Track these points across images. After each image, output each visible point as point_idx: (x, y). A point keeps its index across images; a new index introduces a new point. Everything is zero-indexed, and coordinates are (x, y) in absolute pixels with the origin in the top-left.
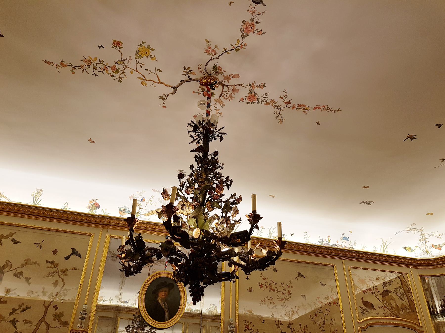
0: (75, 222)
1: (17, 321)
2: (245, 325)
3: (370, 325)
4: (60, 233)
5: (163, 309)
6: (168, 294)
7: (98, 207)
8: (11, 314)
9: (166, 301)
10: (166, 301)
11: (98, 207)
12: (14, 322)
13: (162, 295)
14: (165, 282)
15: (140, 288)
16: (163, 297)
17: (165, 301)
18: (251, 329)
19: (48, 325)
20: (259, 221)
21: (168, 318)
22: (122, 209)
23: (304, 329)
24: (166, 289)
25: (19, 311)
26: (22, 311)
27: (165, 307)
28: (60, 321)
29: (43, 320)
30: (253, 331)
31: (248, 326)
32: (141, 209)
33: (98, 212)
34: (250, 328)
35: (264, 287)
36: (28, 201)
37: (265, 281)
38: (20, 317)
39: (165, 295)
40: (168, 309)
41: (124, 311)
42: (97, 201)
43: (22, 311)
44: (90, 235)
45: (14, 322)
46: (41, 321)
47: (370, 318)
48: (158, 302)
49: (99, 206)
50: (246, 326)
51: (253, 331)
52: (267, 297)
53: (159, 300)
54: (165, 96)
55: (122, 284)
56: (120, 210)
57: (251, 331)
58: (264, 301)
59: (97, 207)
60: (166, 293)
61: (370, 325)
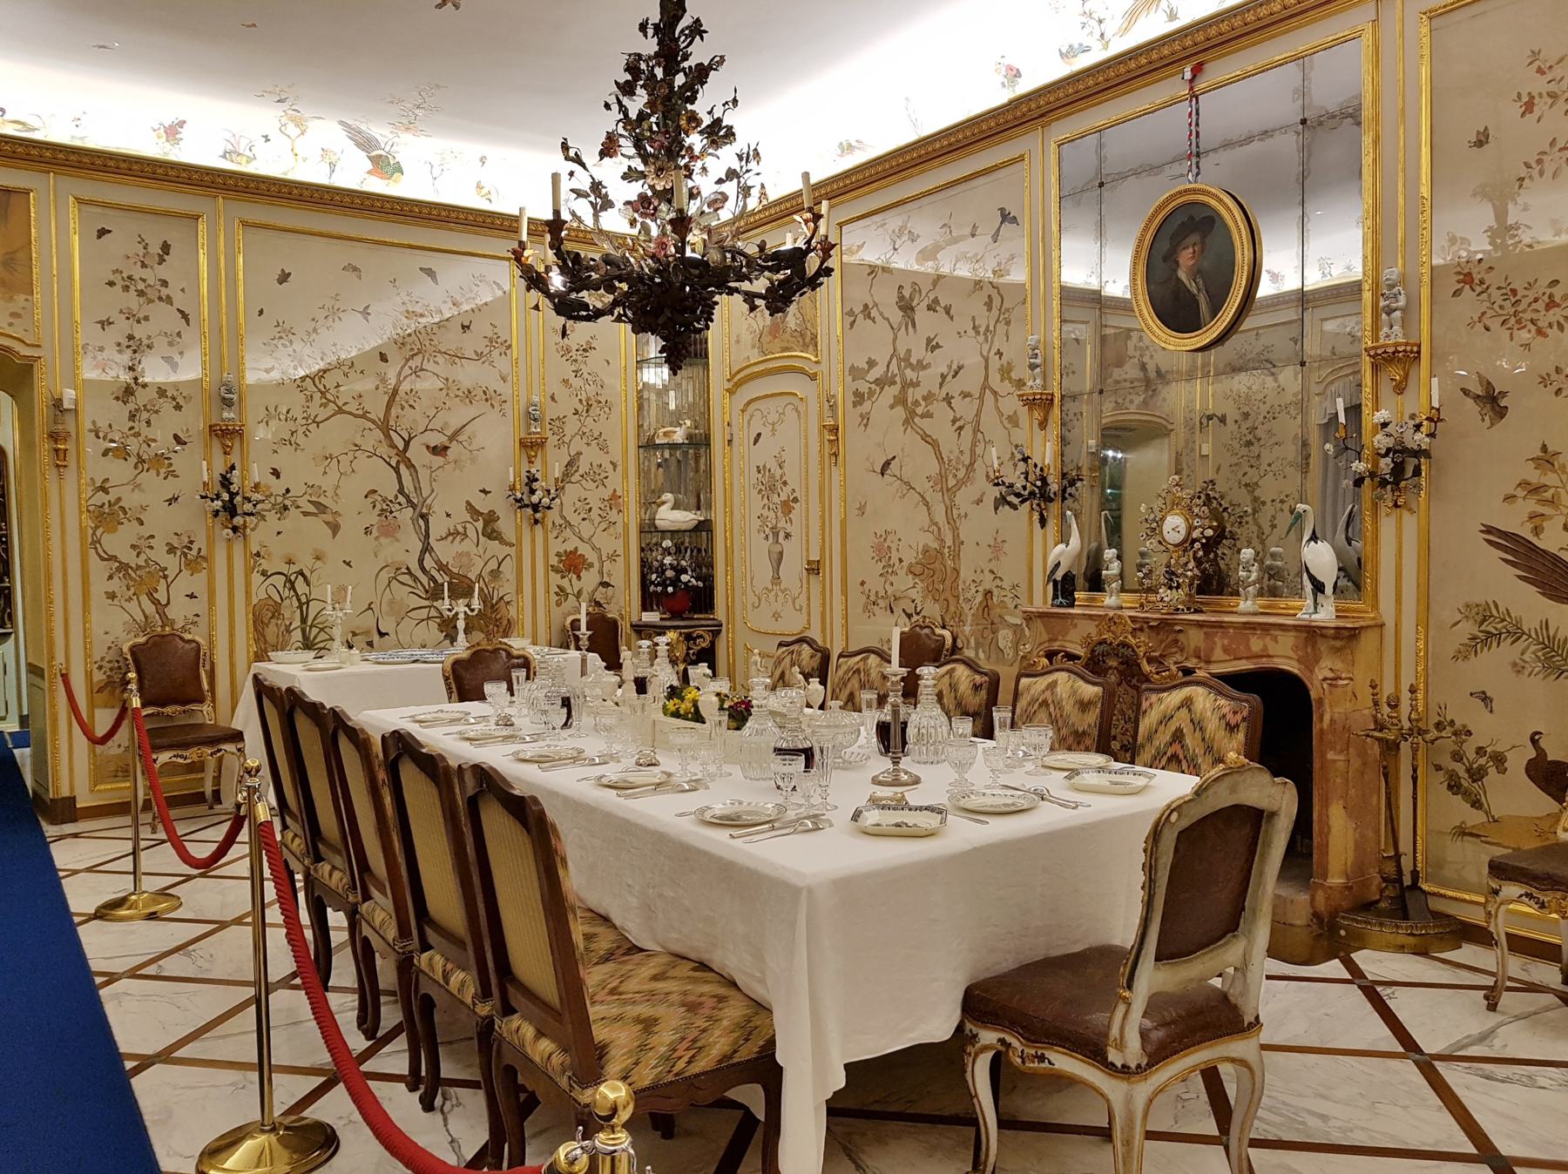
0: (989, 140)
1: (952, 397)
4: (973, 181)
5: (1194, 296)
6: (1202, 251)
7: (1018, 74)
8: (941, 385)
9: (1199, 271)
11: (1018, 74)
12: (948, 399)
13: (1186, 258)
14: (1191, 218)
15: (1137, 231)
17: (1196, 273)
18: (1482, 282)
19: (995, 393)
20: (1461, 947)
21: (1208, 319)
22: (1064, 51)
25: (950, 377)
26: (954, 377)
27: (1199, 290)
28: (1010, 379)
29: (985, 386)
30: (1488, 288)
31: (1470, 274)
32: (1100, 22)
33: (1025, 86)
34: (1477, 277)
35: (1541, 106)
36: (992, 96)
37: (1549, 76)
38: (953, 387)
39: (1193, 258)
40: (1207, 292)
41: (1116, 308)
42: (1006, 61)
43: (954, 377)
44: (1021, 158)
45: (948, 399)
46: (984, 388)
48: (1179, 280)
49: (1018, 70)
50: (1462, 277)
51: (1488, 288)
52: (1551, 144)
53: (1182, 275)
54: (543, 708)
55: (1101, 235)
56: (1061, 54)
57: (1479, 289)
58: (1539, 162)
59: (1015, 76)
60: (1196, 249)
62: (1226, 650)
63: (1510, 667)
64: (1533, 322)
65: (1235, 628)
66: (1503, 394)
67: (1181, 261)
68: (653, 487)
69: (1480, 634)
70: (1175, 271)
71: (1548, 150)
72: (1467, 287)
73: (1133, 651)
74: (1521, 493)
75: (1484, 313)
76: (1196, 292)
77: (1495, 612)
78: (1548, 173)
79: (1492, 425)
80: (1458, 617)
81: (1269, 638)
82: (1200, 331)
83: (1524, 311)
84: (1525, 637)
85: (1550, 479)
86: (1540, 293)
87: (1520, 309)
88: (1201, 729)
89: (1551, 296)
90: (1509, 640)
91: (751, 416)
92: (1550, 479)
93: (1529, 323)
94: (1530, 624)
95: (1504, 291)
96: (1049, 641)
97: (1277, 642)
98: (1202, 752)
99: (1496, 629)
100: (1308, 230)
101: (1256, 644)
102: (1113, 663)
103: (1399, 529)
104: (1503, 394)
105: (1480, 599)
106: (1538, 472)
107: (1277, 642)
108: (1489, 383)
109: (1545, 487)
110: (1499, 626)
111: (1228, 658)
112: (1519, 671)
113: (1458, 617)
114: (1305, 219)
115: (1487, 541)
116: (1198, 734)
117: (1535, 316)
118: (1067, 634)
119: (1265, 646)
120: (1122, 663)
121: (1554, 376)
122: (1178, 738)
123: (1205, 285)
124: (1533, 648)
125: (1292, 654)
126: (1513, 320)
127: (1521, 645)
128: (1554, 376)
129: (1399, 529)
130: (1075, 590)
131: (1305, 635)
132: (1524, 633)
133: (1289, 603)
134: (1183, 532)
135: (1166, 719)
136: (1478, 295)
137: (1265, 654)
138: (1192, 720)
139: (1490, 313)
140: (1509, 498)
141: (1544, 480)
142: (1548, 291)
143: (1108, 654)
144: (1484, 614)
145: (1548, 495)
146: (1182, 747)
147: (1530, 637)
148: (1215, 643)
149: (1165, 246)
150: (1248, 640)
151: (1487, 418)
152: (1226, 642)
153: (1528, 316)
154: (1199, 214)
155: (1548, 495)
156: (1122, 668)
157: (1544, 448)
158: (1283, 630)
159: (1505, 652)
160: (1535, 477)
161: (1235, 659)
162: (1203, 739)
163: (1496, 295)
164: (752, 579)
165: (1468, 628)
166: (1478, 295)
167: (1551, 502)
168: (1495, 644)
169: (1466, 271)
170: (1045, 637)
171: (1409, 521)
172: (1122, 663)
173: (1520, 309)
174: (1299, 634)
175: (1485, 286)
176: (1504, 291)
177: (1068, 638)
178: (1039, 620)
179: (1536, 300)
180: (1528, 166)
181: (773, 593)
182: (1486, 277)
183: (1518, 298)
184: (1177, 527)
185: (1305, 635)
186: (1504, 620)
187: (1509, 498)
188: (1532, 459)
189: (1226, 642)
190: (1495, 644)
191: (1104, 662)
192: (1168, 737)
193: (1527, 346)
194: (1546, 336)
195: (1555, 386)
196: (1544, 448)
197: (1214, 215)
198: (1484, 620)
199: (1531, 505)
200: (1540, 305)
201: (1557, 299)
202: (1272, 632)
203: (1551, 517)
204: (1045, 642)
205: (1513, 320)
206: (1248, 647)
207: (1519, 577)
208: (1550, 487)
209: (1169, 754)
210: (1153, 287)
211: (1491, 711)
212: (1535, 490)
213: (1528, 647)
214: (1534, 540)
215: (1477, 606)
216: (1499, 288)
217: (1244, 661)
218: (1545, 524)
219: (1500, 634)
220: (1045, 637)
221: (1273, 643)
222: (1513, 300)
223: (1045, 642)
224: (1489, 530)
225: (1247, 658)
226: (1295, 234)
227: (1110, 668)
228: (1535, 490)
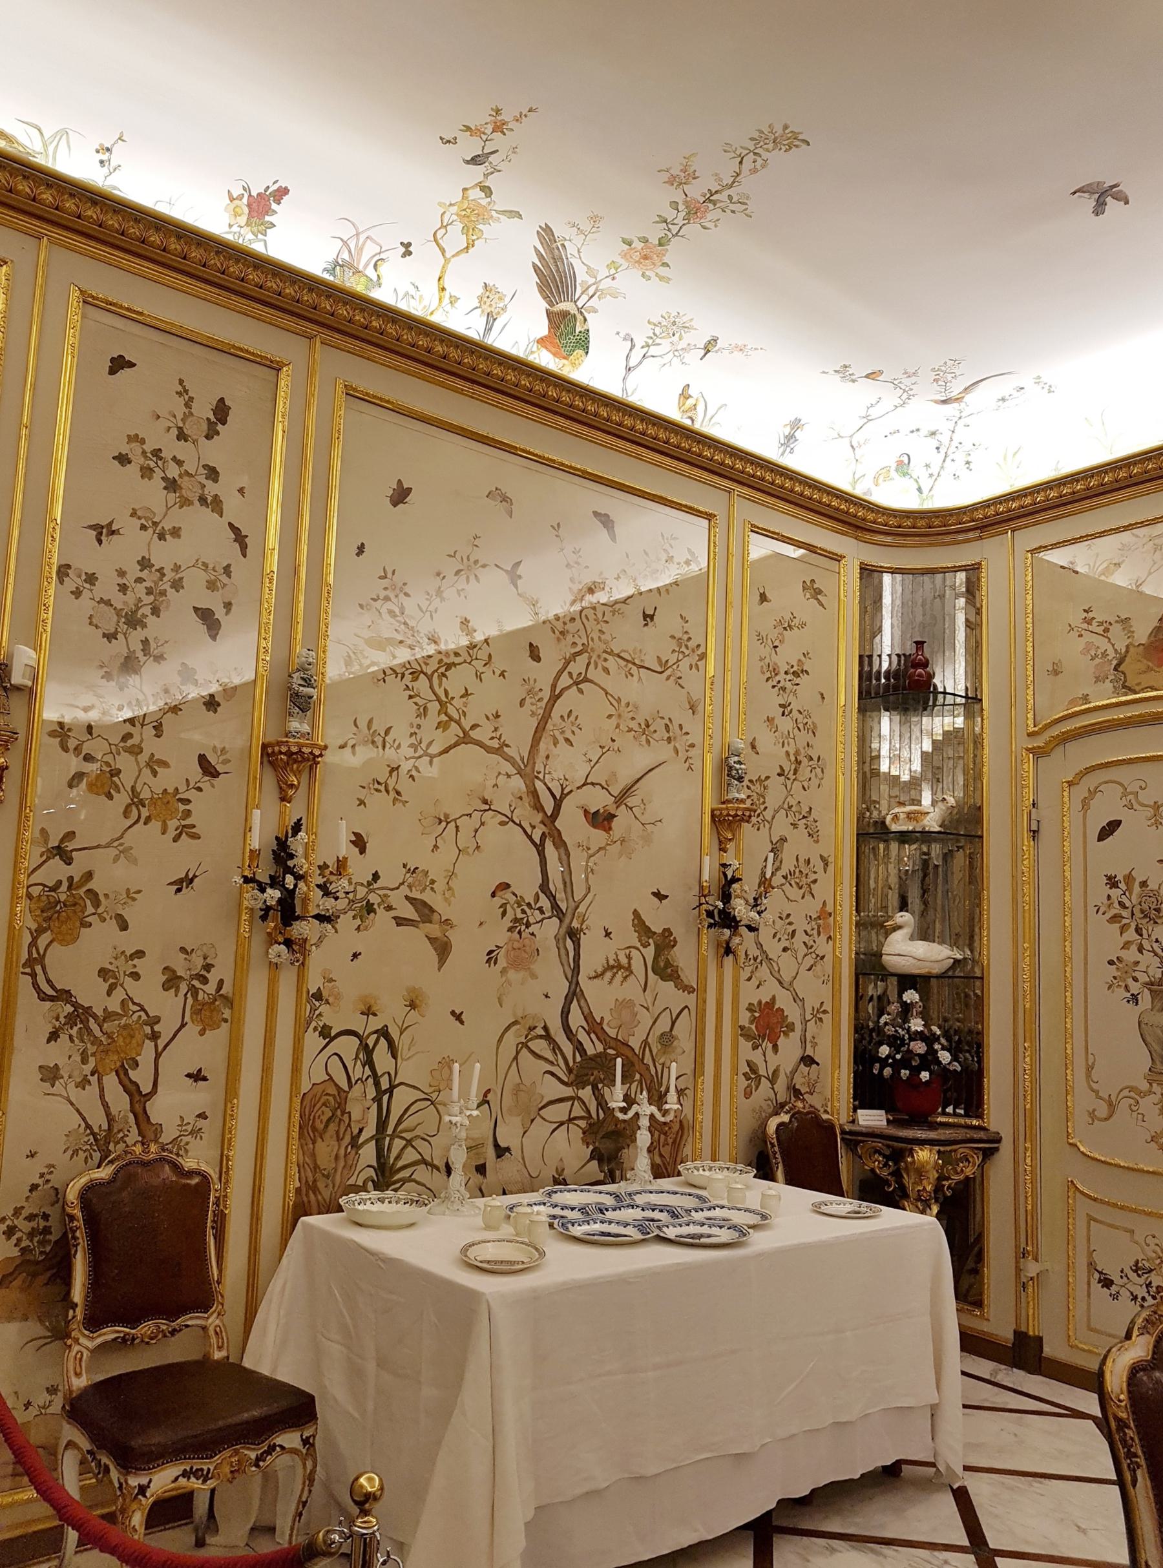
164: (1089, 1069)
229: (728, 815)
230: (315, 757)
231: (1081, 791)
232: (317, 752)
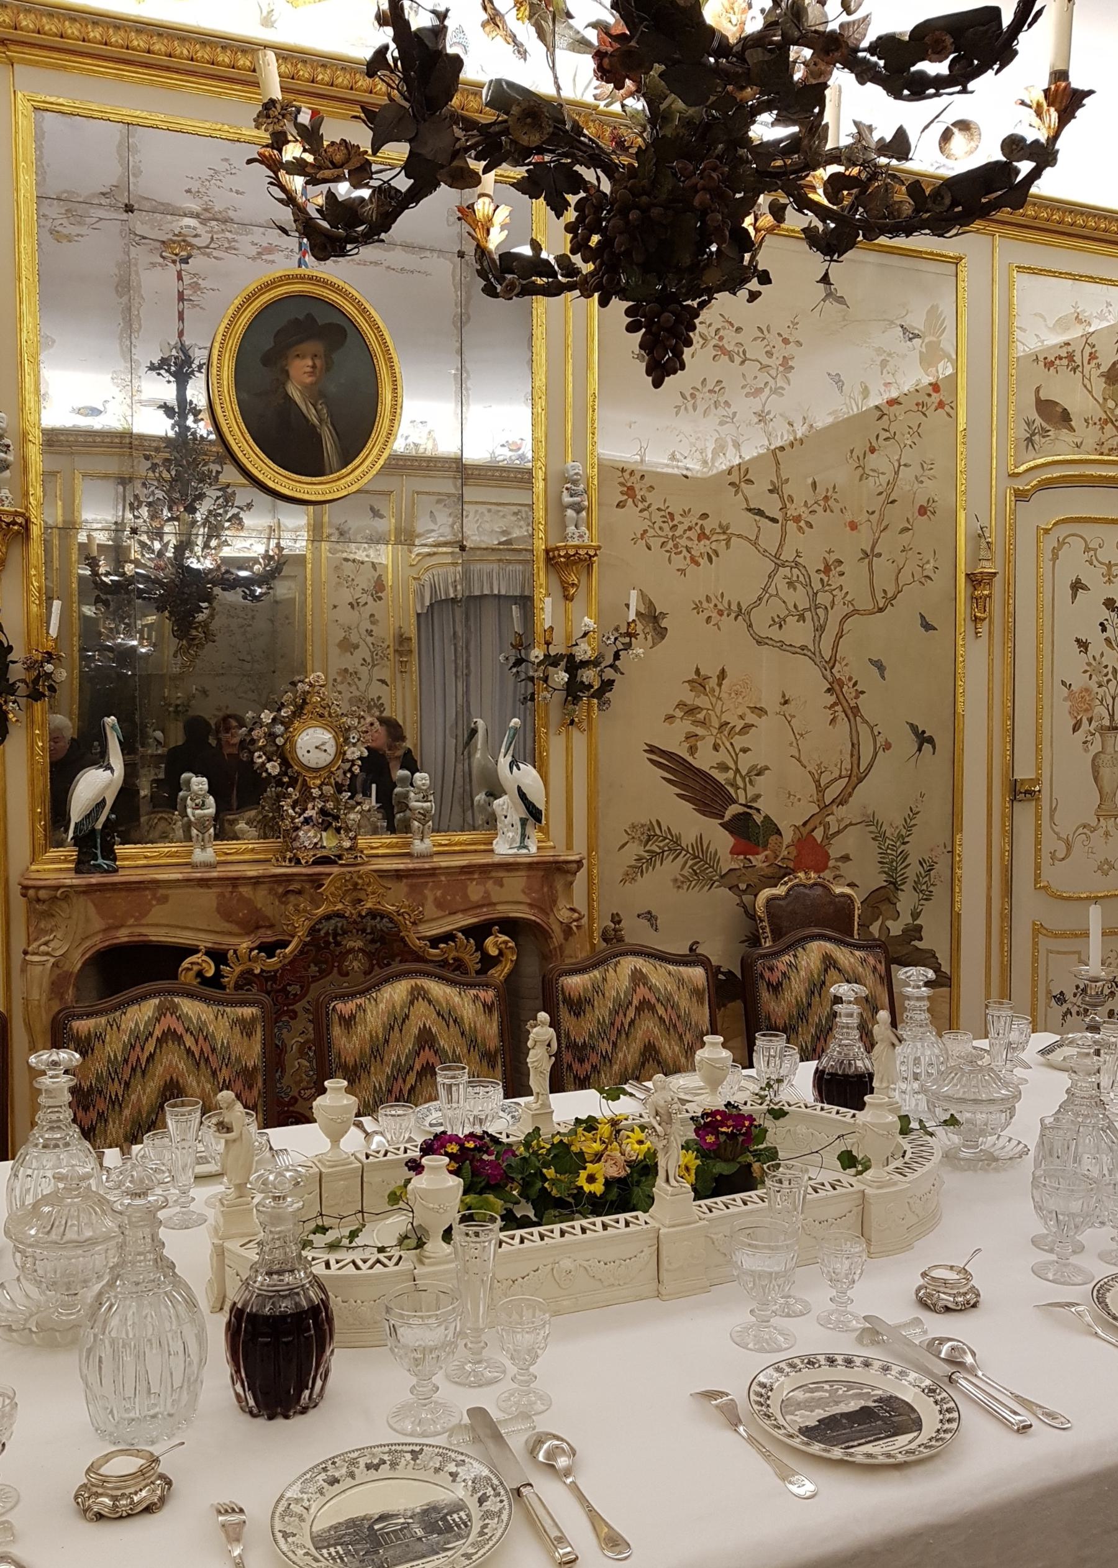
2: (621, 484)
3: (1047, 485)
5: (314, 426)
10: (322, 394)
16: (309, 380)
17: (316, 394)
18: (643, 500)
23: (826, 498)
24: (313, 346)
27: (321, 420)
30: (649, 507)
39: (312, 374)
47: (1050, 459)
53: (294, 391)
57: (641, 506)
58: (693, 396)
61: (1047, 485)
62: (439, 904)
63: (671, 884)
64: (688, 550)
65: (448, 874)
66: (664, 615)
67: (292, 373)
68: (376, 1527)
69: (646, 854)
70: (284, 384)
71: (700, 387)
72: (630, 500)
73: (391, 920)
74: (679, 713)
75: (645, 531)
76: (316, 422)
77: (658, 832)
78: (701, 409)
79: (654, 645)
80: (626, 838)
81: (490, 882)
82: (314, 479)
83: (681, 537)
84: (684, 853)
85: (702, 701)
86: (694, 523)
87: (677, 534)
88: (455, 1021)
89: (702, 527)
90: (671, 857)
91: (1061, 544)
92: (702, 701)
93: (684, 550)
94: (688, 839)
95: (663, 513)
96: (105, 930)
97: (502, 886)
98: (465, 1051)
99: (659, 847)
100: (467, 389)
101: (475, 892)
102: (355, 943)
103: (568, 750)
104: (664, 615)
105: (644, 821)
106: (693, 694)
107: (502, 886)
108: (651, 603)
109: (698, 709)
110: (661, 844)
111: (443, 914)
112: (679, 887)
113: (626, 838)
114: (464, 375)
115: (651, 760)
116: (454, 1029)
117: (689, 544)
118: (144, 914)
119: (486, 892)
120: (373, 941)
121: (705, 605)
122: (426, 1042)
123: (331, 415)
124: (690, 863)
125: (523, 898)
126: (671, 544)
127: (680, 860)
128: (705, 605)
129: (568, 750)
130: (114, 844)
131: (541, 873)
132: (683, 849)
133: (452, 838)
134: (332, 750)
135: (397, 1021)
136: (641, 511)
137: (486, 902)
138: (438, 1014)
139: (651, 532)
140: (670, 718)
141: (698, 702)
142: (700, 522)
143: (345, 932)
144: (650, 833)
145: (701, 716)
146: (436, 1052)
147: (688, 852)
148: (426, 898)
149: (268, 343)
150: (466, 887)
151: (649, 637)
152: (439, 893)
153: (683, 542)
154: (323, 318)
155: (701, 716)
156: (372, 948)
157: (698, 672)
158: (508, 871)
159: (670, 868)
160: (690, 698)
161: (450, 914)
162: (463, 1034)
163: (657, 517)
165: (635, 849)
166: (641, 511)
167: (703, 723)
168: (658, 863)
169: (629, 484)
170: (98, 924)
171: (579, 739)
172: (373, 941)
173: (677, 534)
174: (532, 873)
175: (646, 504)
176: (663, 513)
177: (149, 920)
178: (82, 898)
179: (690, 529)
180: (683, 397)
181: (1101, 832)
182: (648, 495)
183: (675, 522)
184: (323, 744)
185: (541, 873)
186: (666, 838)
187: (670, 718)
188: (688, 681)
189: (439, 893)
190: (658, 863)
191: (338, 944)
192: (410, 1045)
193: (682, 571)
194: (698, 564)
195: (706, 614)
196: (698, 672)
197: (338, 320)
198: (649, 840)
199: (687, 726)
200: (693, 534)
201: (707, 532)
202: (494, 874)
203: (703, 738)
204: (95, 934)
205: (671, 544)
206: (465, 896)
207: (678, 795)
208: (702, 709)
209: (417, 1067)
210: (245, 396)
211: (656, 930)
212: (691, 711)
213: (686, 863)
214: (690, 759)
215: (643, 826)
216: (659, 509)
217: (460, 916)
218: (699, 743)
219: (663, 852)
220: (98, 924)
221: (497, 888)
222: (671, 524)
223: (95, 934)
224: (652, 750)
225: (464, 911)
226: (453, 387)
227: (351, 951)
228: (691, 711)
229: (560, 556)
230: (591, 557)
231: (1050, 542)
232: (592, 553)
